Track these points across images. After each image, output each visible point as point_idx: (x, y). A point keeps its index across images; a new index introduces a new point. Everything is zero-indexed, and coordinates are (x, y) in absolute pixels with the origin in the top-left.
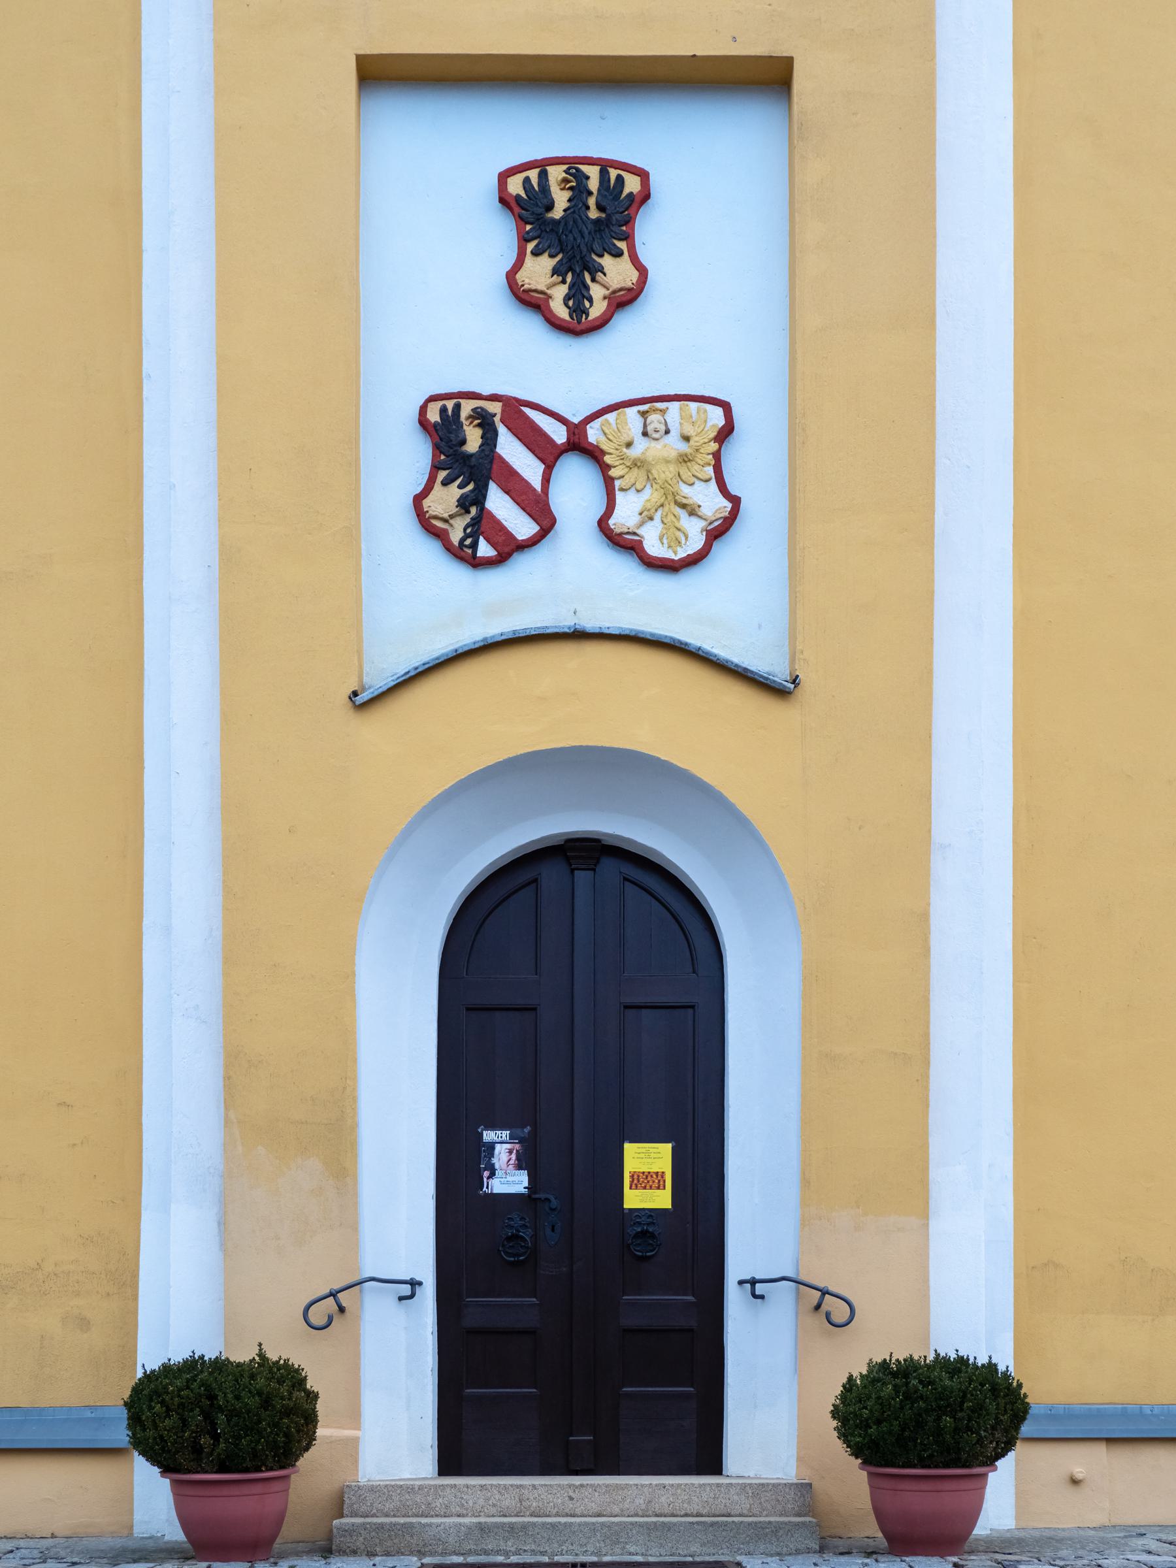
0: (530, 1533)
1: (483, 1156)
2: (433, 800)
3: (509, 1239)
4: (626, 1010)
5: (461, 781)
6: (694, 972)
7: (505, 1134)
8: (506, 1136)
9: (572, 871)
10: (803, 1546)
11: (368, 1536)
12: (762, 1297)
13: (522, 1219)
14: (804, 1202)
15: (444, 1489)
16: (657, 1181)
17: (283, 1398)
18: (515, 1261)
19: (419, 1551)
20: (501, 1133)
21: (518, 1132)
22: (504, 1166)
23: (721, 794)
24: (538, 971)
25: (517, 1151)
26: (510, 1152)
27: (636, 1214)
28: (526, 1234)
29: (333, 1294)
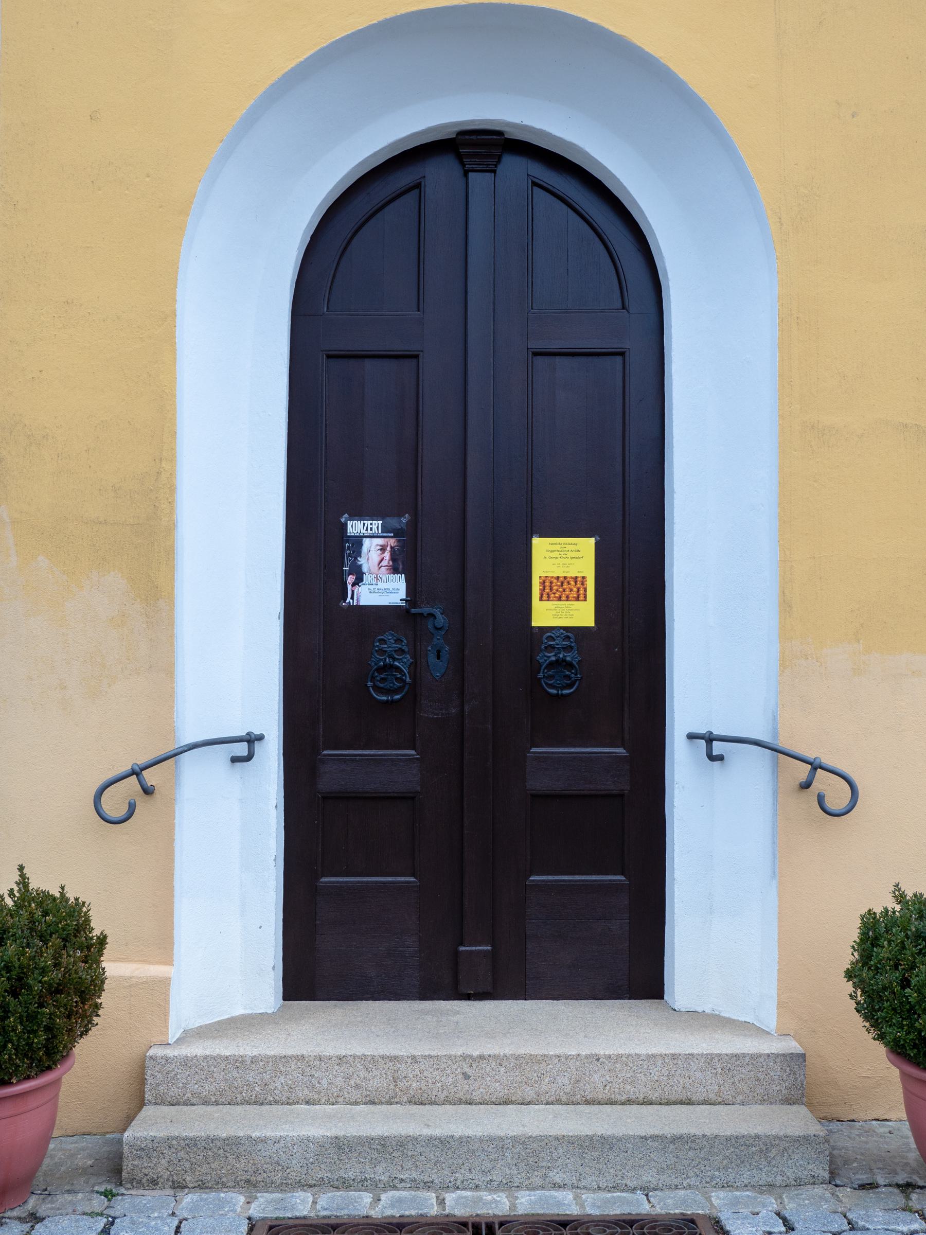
0: (410, 1154)
1: (346, 555)
2: (284, 76)
3: (380, 670)
4: (535, 358)
5: (322, 50)
6: (624, 307)
7: (376, 525)
8: (378, 528)
9: (466, 173)
10: (806, 1173)
11: (173, 1158)
12: (720, 758)
13: (398, 641)
14: (785, 634)
15: (288, 1062)
16: (575, 589)
17: (44, 971)
18: (387, 701)
19: (248, 1181)
20: (371, 524)
21: (394, 522)
22: (375, 569)
23: (669, 69)
24: (421, 306)
25: (391, 548)
26: (383, 549)
27: (549, 634)
28: (403, 663)
29: (136, 772)
